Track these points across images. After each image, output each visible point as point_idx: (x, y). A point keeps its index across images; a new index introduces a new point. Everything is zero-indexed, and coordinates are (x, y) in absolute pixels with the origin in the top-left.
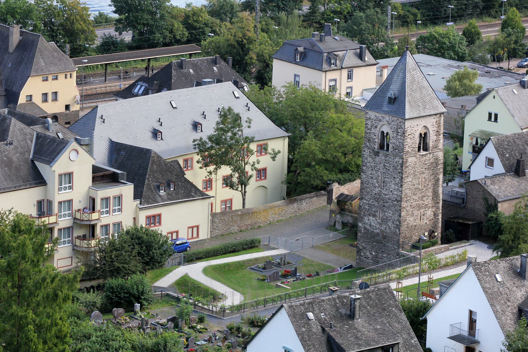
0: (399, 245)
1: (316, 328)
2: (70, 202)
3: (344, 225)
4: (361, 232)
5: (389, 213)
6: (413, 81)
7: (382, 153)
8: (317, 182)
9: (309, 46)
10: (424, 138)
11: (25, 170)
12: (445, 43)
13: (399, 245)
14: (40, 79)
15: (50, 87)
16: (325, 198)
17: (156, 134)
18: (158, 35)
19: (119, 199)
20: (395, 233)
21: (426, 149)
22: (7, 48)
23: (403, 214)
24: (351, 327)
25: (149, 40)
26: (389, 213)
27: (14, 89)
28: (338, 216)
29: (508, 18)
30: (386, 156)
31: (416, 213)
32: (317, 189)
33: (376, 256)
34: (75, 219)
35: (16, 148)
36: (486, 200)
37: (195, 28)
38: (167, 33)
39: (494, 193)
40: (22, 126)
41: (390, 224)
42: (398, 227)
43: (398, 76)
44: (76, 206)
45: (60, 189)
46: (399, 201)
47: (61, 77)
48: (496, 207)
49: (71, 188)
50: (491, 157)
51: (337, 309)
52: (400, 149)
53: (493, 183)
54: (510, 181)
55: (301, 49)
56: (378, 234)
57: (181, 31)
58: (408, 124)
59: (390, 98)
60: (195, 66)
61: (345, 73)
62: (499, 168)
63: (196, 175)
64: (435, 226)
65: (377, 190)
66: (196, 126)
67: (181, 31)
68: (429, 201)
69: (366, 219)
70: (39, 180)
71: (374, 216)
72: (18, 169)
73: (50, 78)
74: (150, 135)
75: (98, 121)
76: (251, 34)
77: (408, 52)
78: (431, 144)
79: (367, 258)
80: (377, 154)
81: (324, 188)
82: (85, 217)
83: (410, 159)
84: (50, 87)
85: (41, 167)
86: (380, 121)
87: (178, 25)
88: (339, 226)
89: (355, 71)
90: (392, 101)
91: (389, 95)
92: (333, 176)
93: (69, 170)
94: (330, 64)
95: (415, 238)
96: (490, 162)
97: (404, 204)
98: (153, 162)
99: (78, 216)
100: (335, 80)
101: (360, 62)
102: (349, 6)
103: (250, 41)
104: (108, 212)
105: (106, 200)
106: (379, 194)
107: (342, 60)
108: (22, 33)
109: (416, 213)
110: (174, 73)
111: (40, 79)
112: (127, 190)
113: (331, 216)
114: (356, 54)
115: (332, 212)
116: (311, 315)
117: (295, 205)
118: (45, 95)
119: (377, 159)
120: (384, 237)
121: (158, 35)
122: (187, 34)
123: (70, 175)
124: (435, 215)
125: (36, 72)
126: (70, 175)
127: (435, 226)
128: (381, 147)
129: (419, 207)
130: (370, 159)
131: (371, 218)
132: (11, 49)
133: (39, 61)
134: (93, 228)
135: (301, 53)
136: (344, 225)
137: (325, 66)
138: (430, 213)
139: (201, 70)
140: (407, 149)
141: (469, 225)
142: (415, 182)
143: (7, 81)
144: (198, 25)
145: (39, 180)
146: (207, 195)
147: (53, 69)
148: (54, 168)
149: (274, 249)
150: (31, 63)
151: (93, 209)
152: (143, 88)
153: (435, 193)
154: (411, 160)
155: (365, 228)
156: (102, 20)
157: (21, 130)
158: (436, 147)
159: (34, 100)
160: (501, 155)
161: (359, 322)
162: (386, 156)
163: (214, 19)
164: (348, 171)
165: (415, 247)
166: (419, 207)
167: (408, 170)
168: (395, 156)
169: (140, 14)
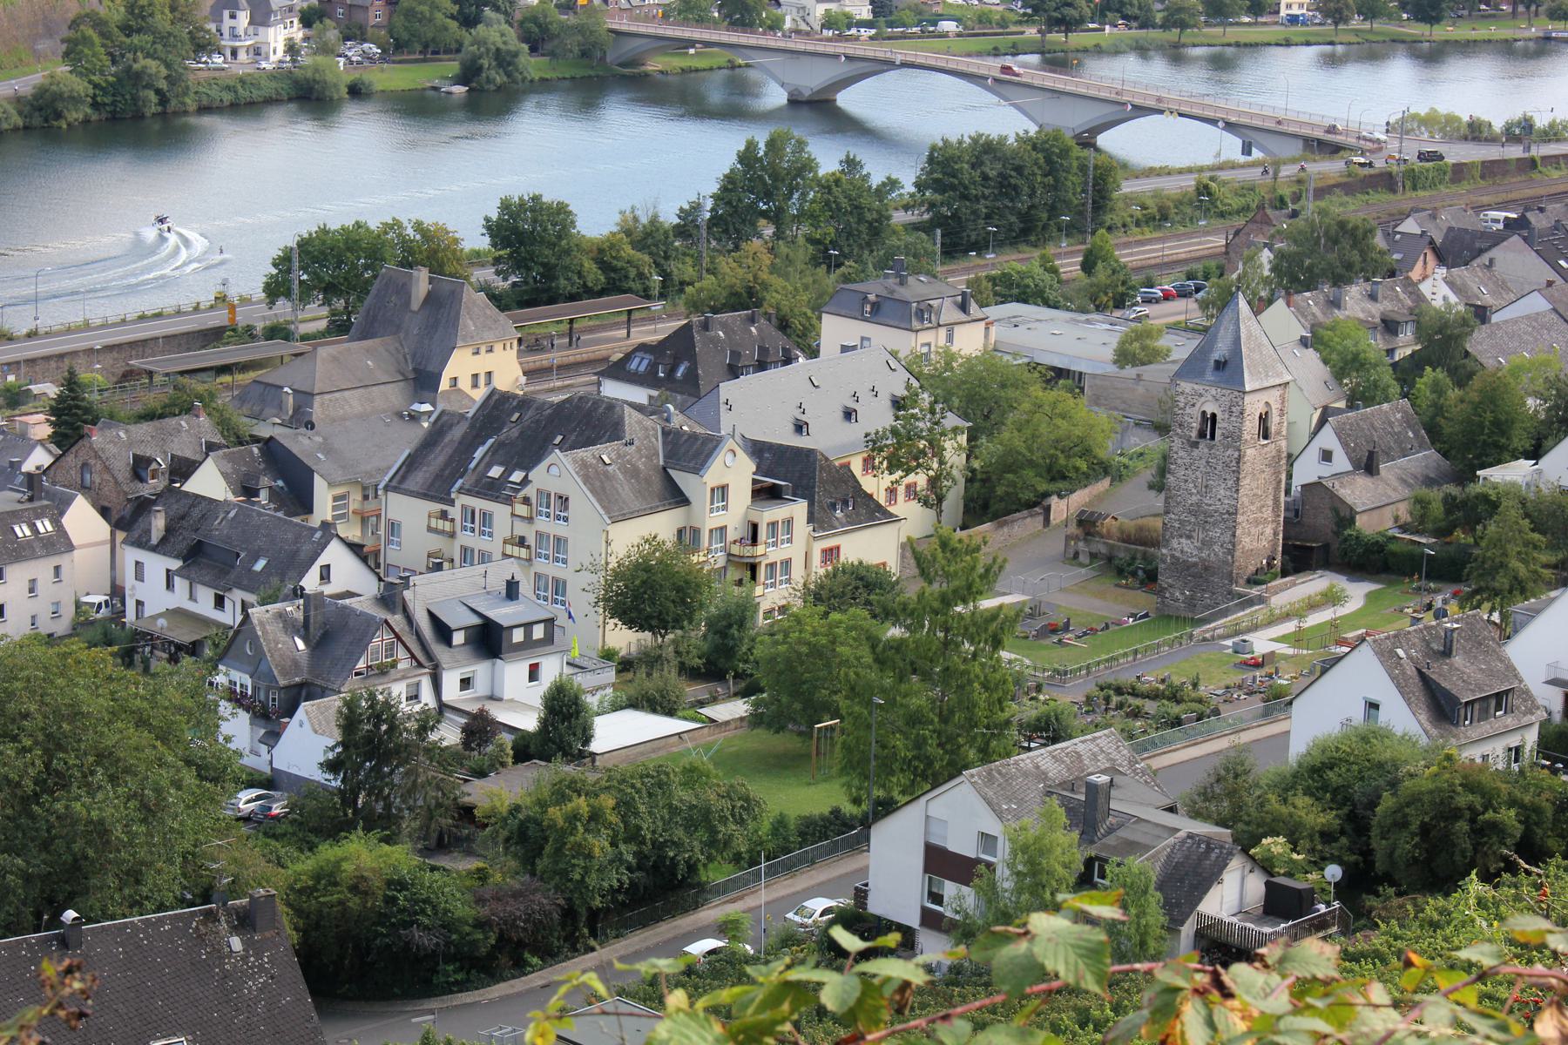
0: (1231, 579)
1: (1411, 671)
2: (723, 529)
3: (1093, 556)
4: (1164, 562)
5: (1215, 533)
6: (1250, 336)
7: (1203, 444)
8: (1027, 495)
9: (884, 293)
10: (1264, 419)
11: (657, 482)
12: (1028, 286)
13: (1231, 579)
14: (470, 351)
15: (482, 363)
16: (1041, 518)
17: (800, 427)
18: (562, 282)
19: (789, 522)
20: (1225, 562)
21: (1266, 437)
22: (408, 303)
23: (1238, 532)
24: (1451, 666)
25: (550, 289)
26: (1215, 533)
27: (430, 368)
28: (1081, 544)
29: (1094, 245)
30: (1211, 448)
31: (1253, 530)
32: (1030, 505)
33: (1192, 598)
34: (729, 555)
35: (639, 450)
36: (1336, 511)
37: (614, 270)
38: (576, 278)
39: (1349, 500)
40: (640, 416)
41: (1216, 548)
42: (1231, 552)
43: (1226, 329)
44: (732, 535)
45: (711, 511)
46: (1233, 513)
47: (498, 347)
48: (1352, 521)
49: (725, 508)
50: (1327, 447)
51: (1428, 644)
52: (1235, 438)
53: (1342, 485)
54: (1362, 481)
55: (872, 297)
56: (1195, 564)
57: (594, 275)
58: (1247, 399)
59: (1217, 362)
60: (724, 326)
61: (943, 332)
62: (1341, 462)
63: (875, 485)
64: (1274, 550)
65: (1195, 499)
66: (849, 414)
67: (594, 275)
68: (1268, 513)
69: (1174, 543)
70: (678, 498)
71: (1189, 537)
72: (648, 481)
73: (483, 349)
74: (791, 427)
75: (723, 408)
76: (764, 276)
77: (1240, 295)
78: (1273, 429)
79: (1177, 600)
80: (1195, 445)
81: (1038, 503)
82: (748, 551)
83: (1249, 452)
84: (482, 363)
85: (682, 479)
86: (1201, 395)
87: (589, 265)
88: (1083, 558)
89: (956, 328)
90: (1220, 365)
91: (1216, 356)
92: (1052, 487)
93: (724, 482)
94: (922, 319)
95: (1252, 569)
96: (1327, 456)
97: (1240, 518)
98: (822, 468)
99: (735, 550)
100: (929, 345)
101: (963, 317)
102: (832, 230)
103: (766, 286)
104: (775, 544)
105: (773, 525)
106: (1198, 505)
107: (938, 314)
108: (431, 280)
109: (1253, 530)
110: (697, 337)
111: (470, 351)
112: (798, 510)
113: (1067, 545)
114: (955, 303)
115: (1068, 538)
116: (1400, 652)
117: (1005, 529)
118: (475, 376)
119: (1196, 452)
120: (1206, 569)
121: (562, 282)
122: (602, 278)
123: (724, 489)
124: (1275, 534)
125: (464, 340)
126: (724, 489)
127: (1274, 550)
128: (1202, 435)
129: (1257, 522)
130: (1181, 453)
131: (1183, 540)
132: (415, 305)
133: (467, 323)
134: (753, 568)
135: (873, 304)
136: (1093, 556)
137: (916, 324)
138: (1269, 531)
139: (734, 333)
140: (1246, 436)
141: (1312, 548)
142: (1254, 485)
143: (414, 356)
144: (620, 264)
145: (678, 498)
146: (891, 515)
147: (489, 336)
148: (705, 479)
149: (1004, 594)
150: (455, 326)
151: (754, 540)
152: (645, 362)
153: (1276, 500)
154: (1250, 453)
155: (1173, 556)
156: (476, 258)
157: (639, 422)
158: (1278, 433)
159: (460, 385)
160: (1345, 445)
161: (1457, 660)
162: (1211, 448)
163: (639, 255)
164: (1064, 478)
165: (1252, 582)
166: (1257, 522)
167: (1246, 468)
168: (1227, 447)
169: (536, 248)
